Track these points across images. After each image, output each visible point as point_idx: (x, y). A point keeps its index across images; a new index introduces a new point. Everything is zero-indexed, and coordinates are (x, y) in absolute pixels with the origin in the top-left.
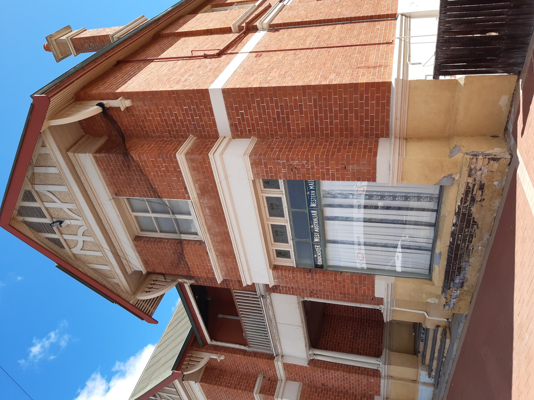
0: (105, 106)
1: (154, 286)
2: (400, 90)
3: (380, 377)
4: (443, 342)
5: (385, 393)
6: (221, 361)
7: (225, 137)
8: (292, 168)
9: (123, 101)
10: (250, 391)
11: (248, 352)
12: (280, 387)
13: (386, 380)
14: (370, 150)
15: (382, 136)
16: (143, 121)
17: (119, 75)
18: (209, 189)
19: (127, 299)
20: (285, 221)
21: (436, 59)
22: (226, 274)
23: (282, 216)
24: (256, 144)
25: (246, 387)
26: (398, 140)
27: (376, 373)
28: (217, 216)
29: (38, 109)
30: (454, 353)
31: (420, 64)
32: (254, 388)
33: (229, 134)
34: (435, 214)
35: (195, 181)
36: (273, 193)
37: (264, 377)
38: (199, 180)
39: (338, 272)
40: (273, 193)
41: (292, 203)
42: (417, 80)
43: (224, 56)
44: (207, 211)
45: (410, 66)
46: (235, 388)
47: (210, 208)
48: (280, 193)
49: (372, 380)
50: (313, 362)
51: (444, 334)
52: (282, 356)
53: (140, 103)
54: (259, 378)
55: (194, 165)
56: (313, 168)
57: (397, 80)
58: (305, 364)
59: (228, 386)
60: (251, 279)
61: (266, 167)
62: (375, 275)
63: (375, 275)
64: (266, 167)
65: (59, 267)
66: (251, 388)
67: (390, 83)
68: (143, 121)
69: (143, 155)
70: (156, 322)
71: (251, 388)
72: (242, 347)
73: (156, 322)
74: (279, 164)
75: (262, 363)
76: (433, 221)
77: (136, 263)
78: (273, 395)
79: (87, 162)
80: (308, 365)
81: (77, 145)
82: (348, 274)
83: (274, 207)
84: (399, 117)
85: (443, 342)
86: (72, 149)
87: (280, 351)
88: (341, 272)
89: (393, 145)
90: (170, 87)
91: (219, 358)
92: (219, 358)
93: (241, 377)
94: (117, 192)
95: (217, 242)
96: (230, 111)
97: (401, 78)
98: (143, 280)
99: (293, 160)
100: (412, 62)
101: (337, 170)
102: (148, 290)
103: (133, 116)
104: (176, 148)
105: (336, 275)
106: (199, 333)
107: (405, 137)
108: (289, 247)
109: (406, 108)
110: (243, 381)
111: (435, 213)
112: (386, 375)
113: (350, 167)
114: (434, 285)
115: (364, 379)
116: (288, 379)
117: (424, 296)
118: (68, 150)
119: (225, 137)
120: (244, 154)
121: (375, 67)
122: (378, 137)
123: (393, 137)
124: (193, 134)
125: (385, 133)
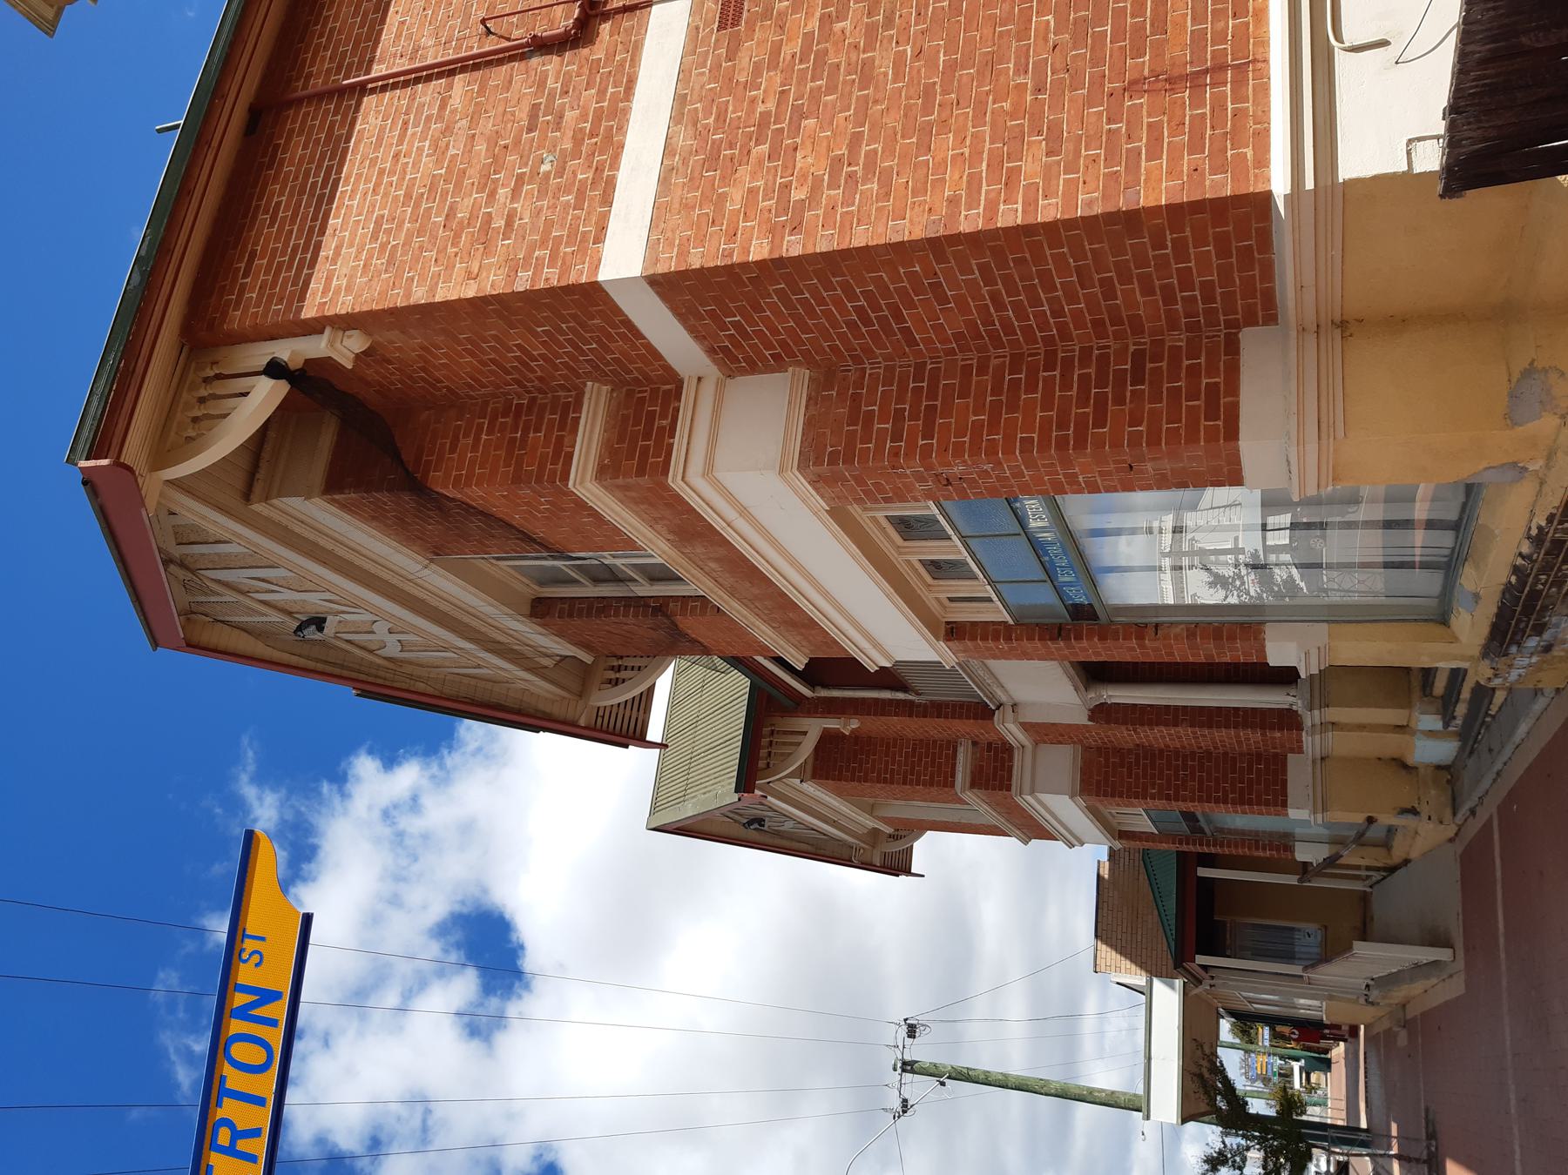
0: (292, 366)
1: (623, 675)
2: (1308, 231)
3: (1300, 727)
5: (1309, 297)
6: (853, 731)
7: (699, 379)
9: (338, 345)
10: (945, 785)
11: (919, 705)
12: (1021, 766)
13: (1317, 737)
15: (1251, 321)
16: (423, 369)
17: (280, 196)
19: (570, 715)
21: (1463, 56)
24: (809, 399)
25: (932, 777)
26: (1311, 340)
27: (1292, 929)
29: (112, 502)
31: (1383, 43)
32: (953, 776)
33: (710, 370)
37: (975, 743)
39: (1146, 625)
42: (1376, 178)
43: (605, 28)
45: (1343, 61)
46: (905, 783)
49: (1278, 735)
50: (1101, 713)
52: (1014, 706)
53: (394, 335)
54: (961, 750)
57: (1294, 198)
58: (1082, 718)
59: (885, 781)
62: (1264, 623)
63: (1264, 623)
65: (364, 694)
66: (946, 778)
67: (1268, 196)
68: (423, 369)
69: (469, 476)
71: (946, 778)
72: (901, 696)
75: (962, 727)
76: (1453, 516)
78: (1009, 789)
80: (1090, 719)
81: (263, 465)
82: (1178, 630)
84: (1309, 278)
86: (258, 488)
87: (1004, 698)
88: (1157, 626)
89: (1293, 343)
90: (470, 276)
91: (849, 725)
92: (849, 725)
93: (914, 750)
94: (436, 551)
96: (692, 321)
97: (1310, 184)
100: (1352, 35)
102: (612, 675)
103: (389, 362)
104: (560, 440)
105: (1140, 637)
106: (774, 686)
107: (1338, 318)
109: (1338, 254)
110: (920, 760)
112: (1317, 721)
114: (1454, 639)
115: (1253, 738)
118: (247, 496)
119: (699, 379)
120: (781, 471)
121: (1196, 81)
123: (1294, 334)
124: (595, 380)
125: (1265, 311)
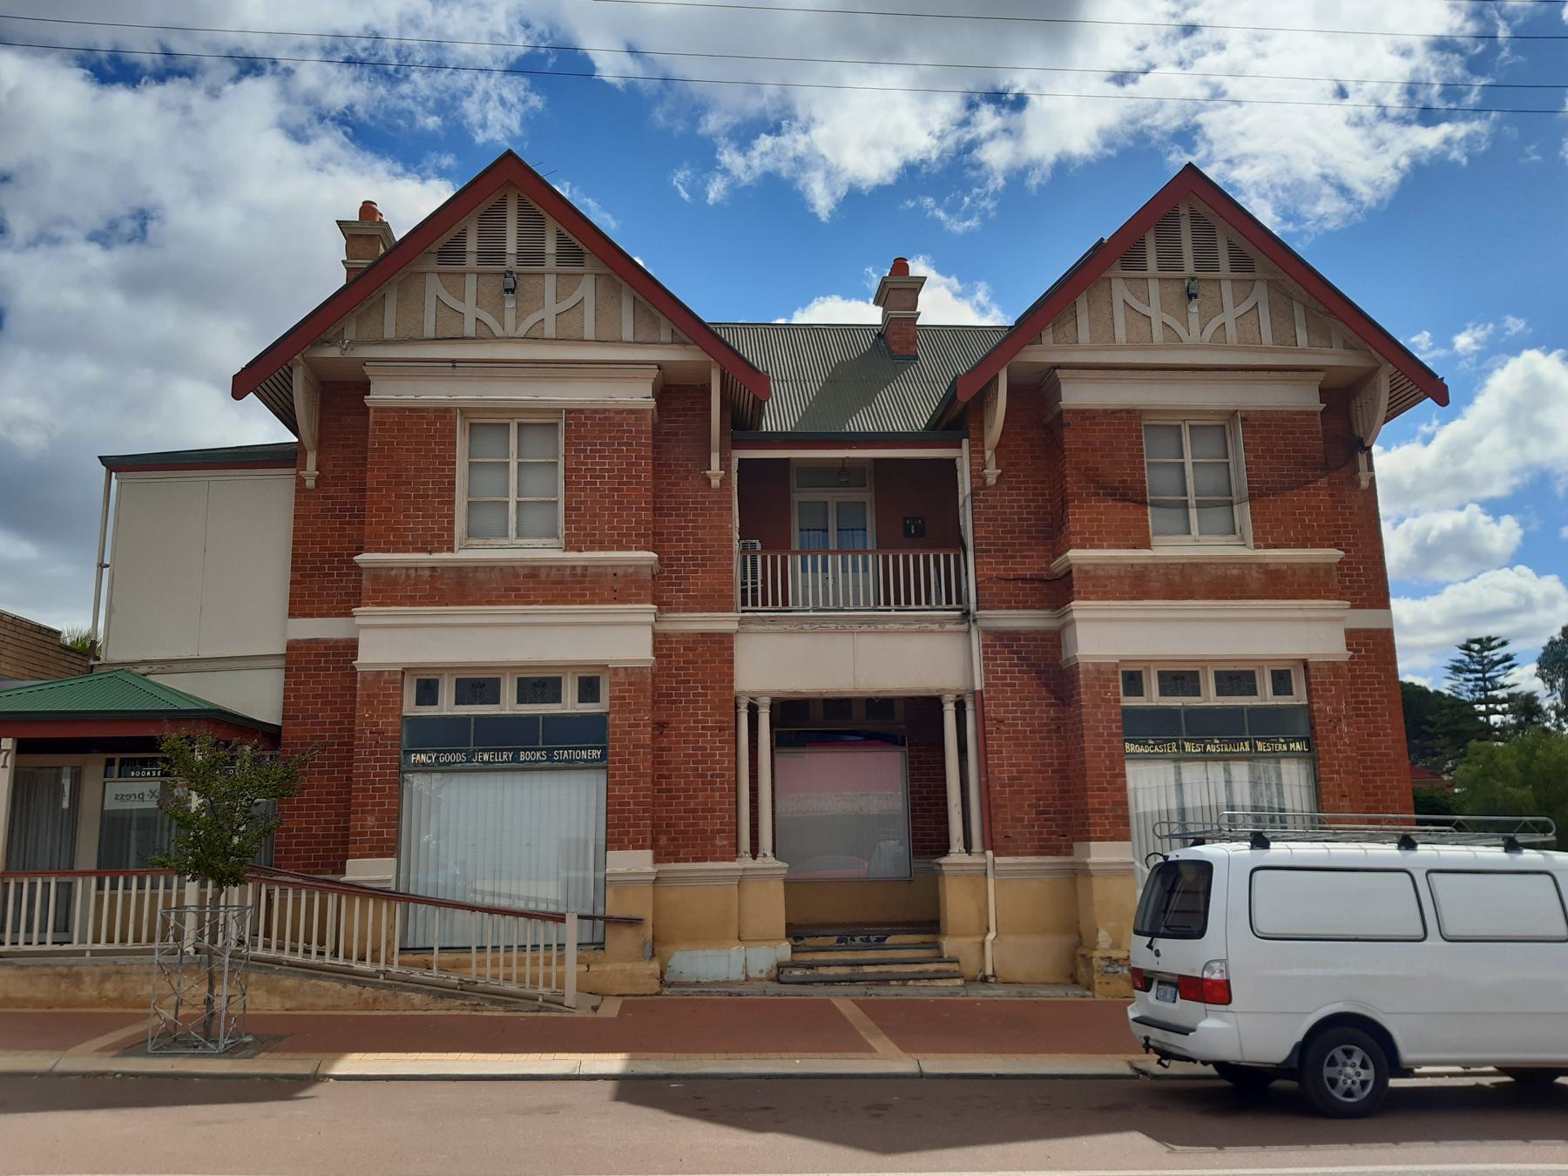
14: (1042, 847)
18: (1278, 585)
22: (1087, 572)
23: (459, 701)
28: (1181, 583)
30: (1042, 992)
34: (743, 977)
38: (1294, 573)
41: (1192, 712)
44: (1235, 572)
55: (1321, 573)
56: (1339, 751)
60: (1083, 620)
61: (1331, 683)
64: (1331, 683)
74: (1339, 703)
76: (751, 975)
77: (1077, 395)
79: (1303, 398)
95: (1167, 574)
99: (1348, 725)
101: (1340, 786)
117: (1112, 924)
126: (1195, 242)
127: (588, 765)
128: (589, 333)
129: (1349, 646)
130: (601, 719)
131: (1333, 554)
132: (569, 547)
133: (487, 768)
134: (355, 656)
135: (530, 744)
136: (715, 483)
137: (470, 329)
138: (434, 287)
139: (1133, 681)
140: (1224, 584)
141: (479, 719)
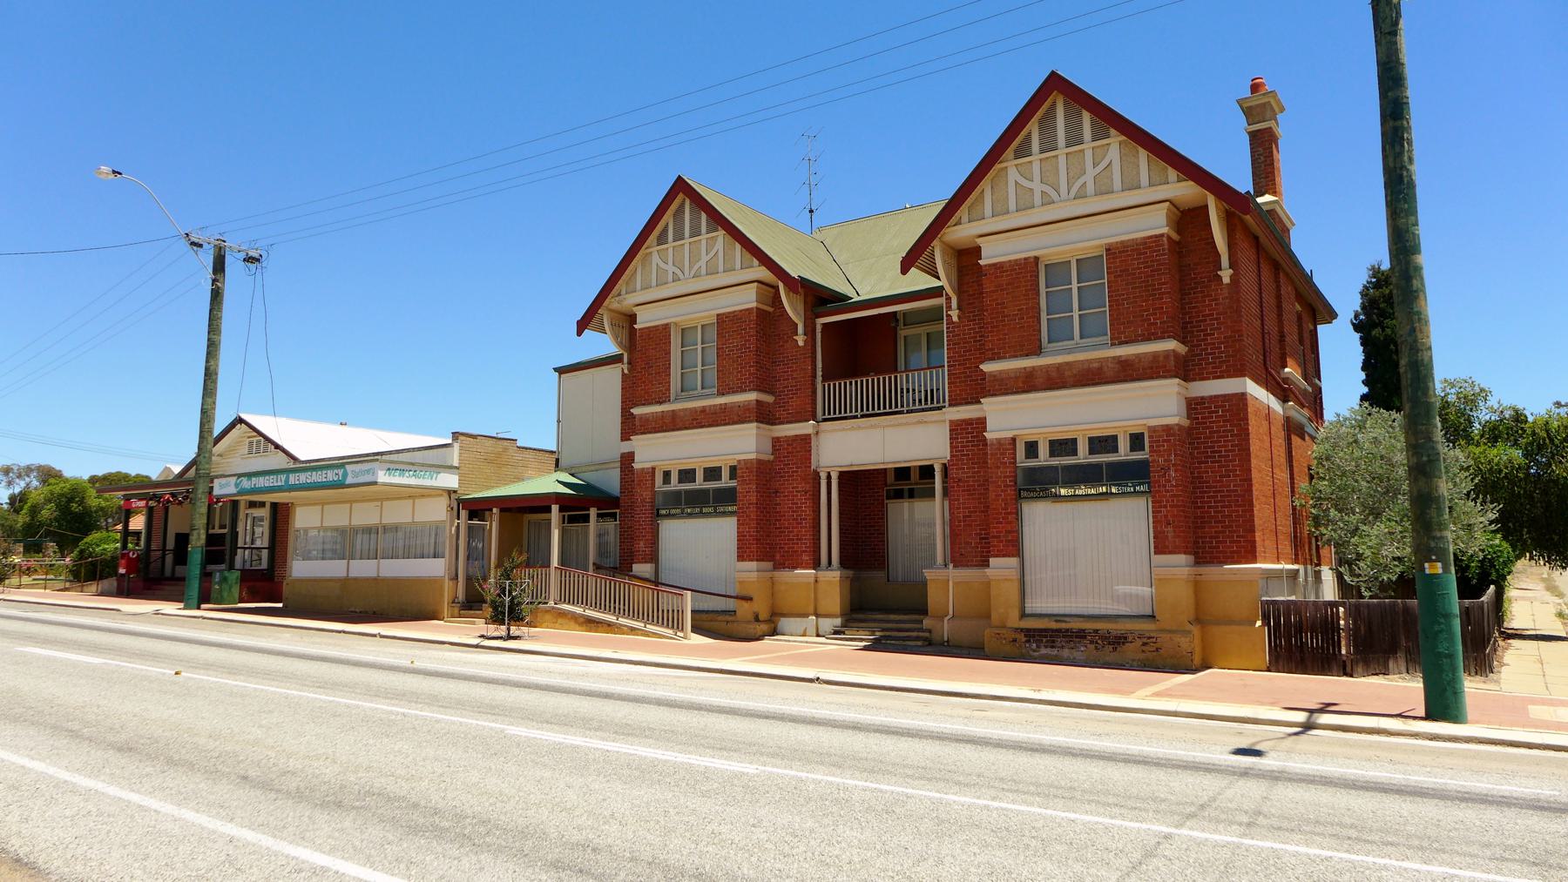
4: (917, 638)
8: (1165, 470)
18: (1127, 372)
20: (699, 483)
28: (1056, 380)
35: (1137, 356)
36: (725, 474)
40: (725, 474)
41: (717, 491)
47: (1100, 369)
48: (725, 482)
51: (925, 639)
70: (579, 333)
73: (579, 333)
77: (992, 253)
79: (1156, 223)
83: (713, 473)
85: (917, 638)
98: (966, 257)
108: (675, 485)
111: (1028, 611)
113: (1170, 529)
116: (776, 441)
122: (1196, 554)
126: (1066, 116)
127: (732, 513)
128: (1117, 184)
129: (1189, 417)
130: (1143, 464)
131: (1171, 345)
132: (1117, 341)
133: (690, 515)
134: (984, 429)
135: (706, 503)
136: (1226, 280)
137: (1037, 200)
138: (1013, 175)
139: (1032, 449)
140: (1090, 376)
141: (686, 492)
